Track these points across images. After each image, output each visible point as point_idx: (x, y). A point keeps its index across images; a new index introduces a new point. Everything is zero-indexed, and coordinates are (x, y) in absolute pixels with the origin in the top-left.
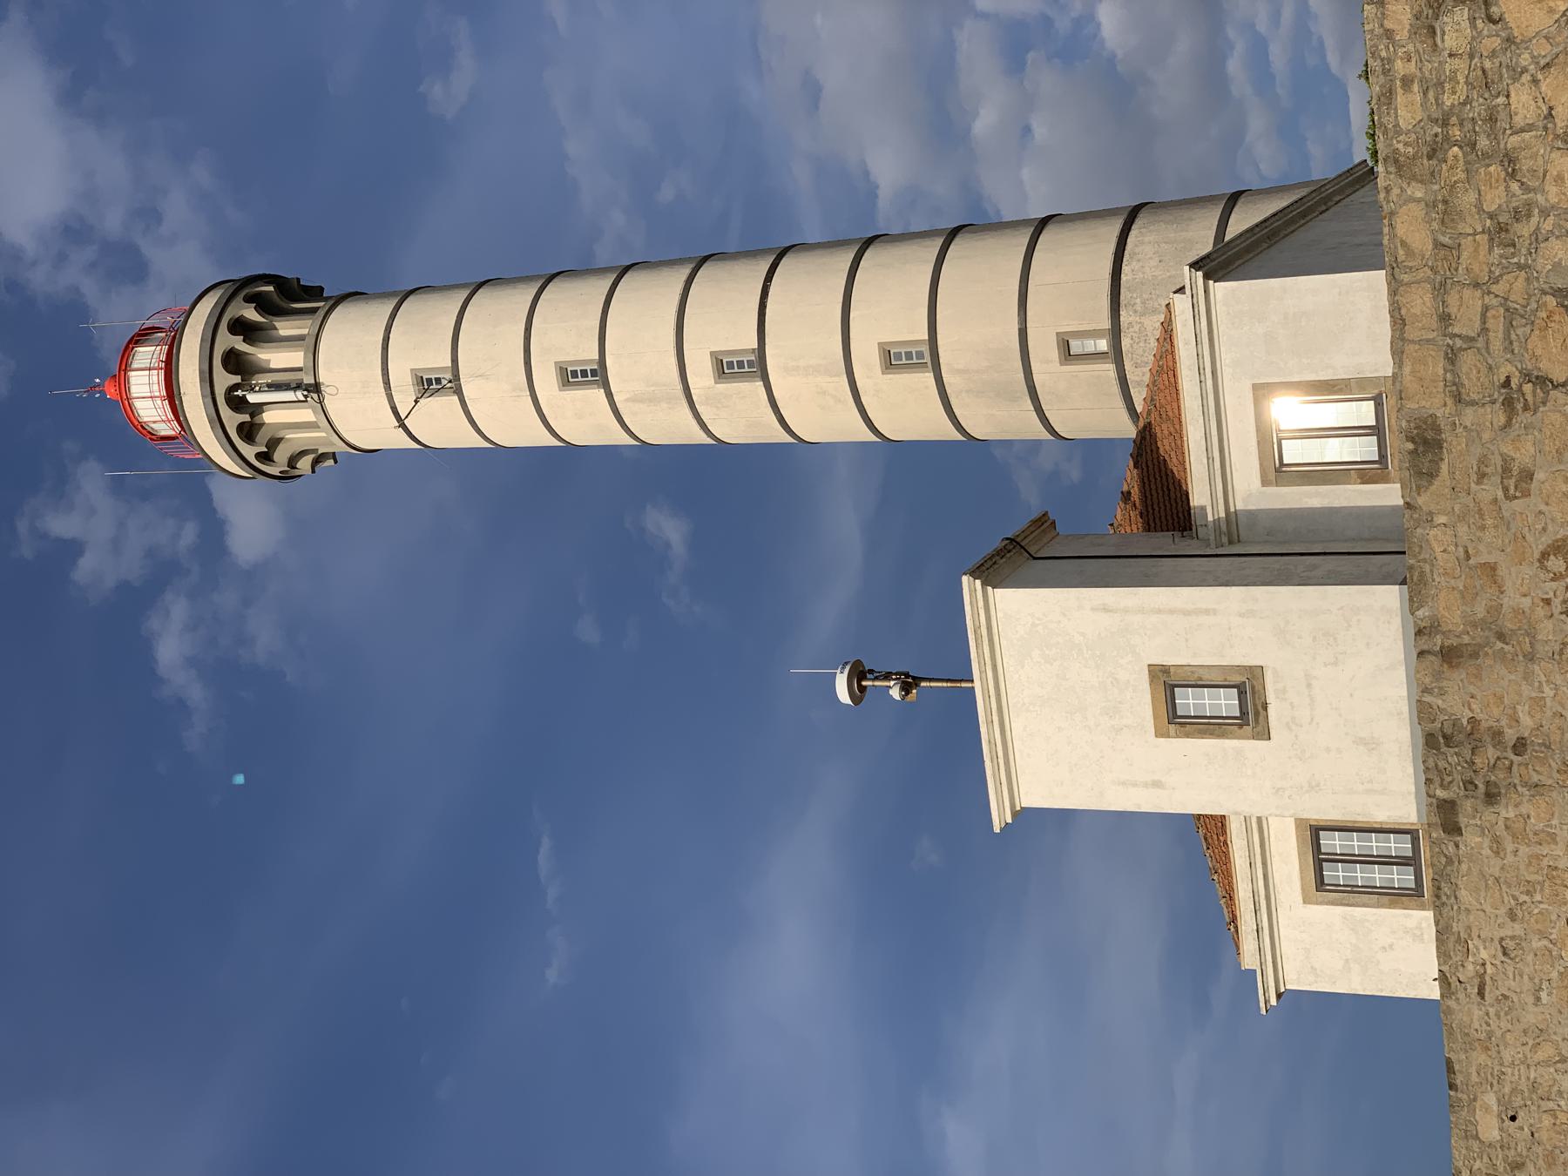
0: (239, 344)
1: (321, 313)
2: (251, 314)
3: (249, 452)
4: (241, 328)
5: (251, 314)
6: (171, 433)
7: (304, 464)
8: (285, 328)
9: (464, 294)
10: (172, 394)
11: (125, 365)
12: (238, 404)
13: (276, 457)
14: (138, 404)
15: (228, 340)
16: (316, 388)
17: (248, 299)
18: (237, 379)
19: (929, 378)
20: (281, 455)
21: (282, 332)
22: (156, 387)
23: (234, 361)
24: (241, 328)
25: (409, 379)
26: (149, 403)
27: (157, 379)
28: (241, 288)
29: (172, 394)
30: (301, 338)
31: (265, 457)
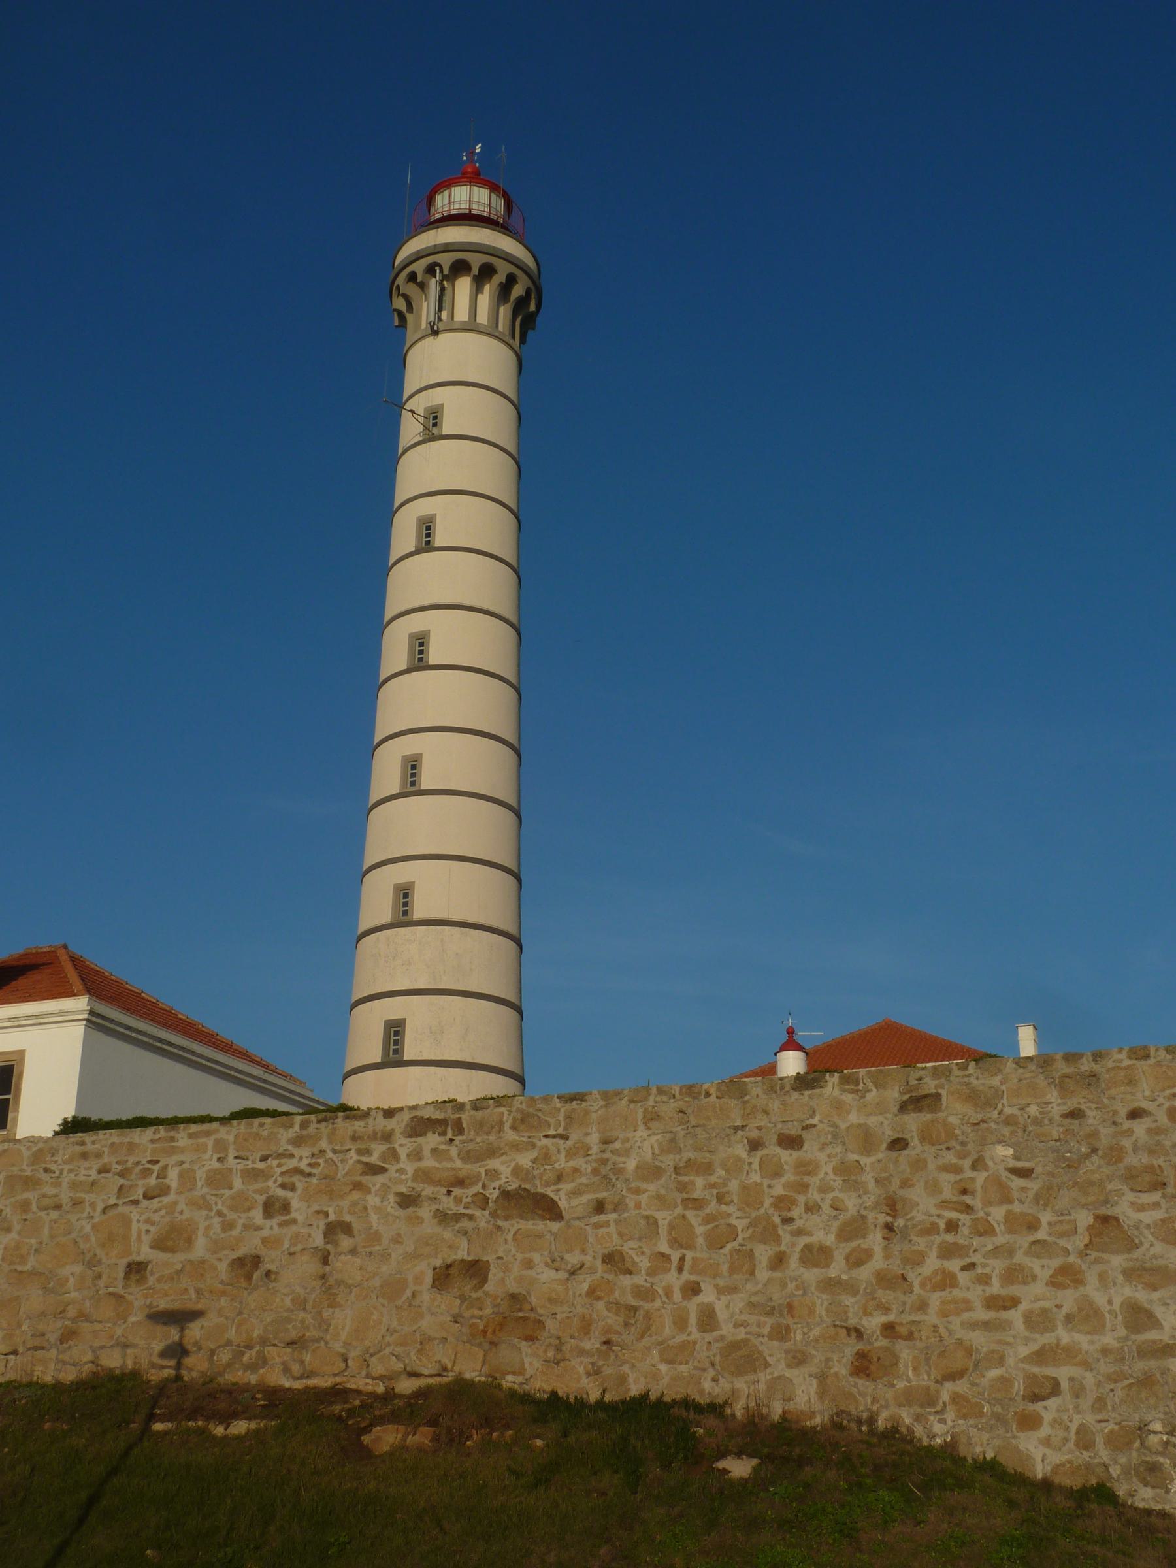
0: (500, 278)
1: (511, 341)
2: (518, 291)
3: (419, 267)
4: (511, 280)
5: (518, 291)
6: (432, 211)
7: (399, 304)
8: (505, 312)
9: (514, 452)
10: (469, 219)
11: (494, 188)
12: (430, 270)
13: (411, 285)
14: (446, 193)
15: (503, 270)
16: (435, 333)
17: (528, 291)
18: (446, 272)
19: (396, 791)
20: (411, 290)
21: (502, 309)
22: (456, 207)
23: (487, 272)
24: (511, 280)
25: (436, 402)
26: (446, 201)
27: (480, 209)
28: (536, 290)
29: (469, 219)
30: (497, 326)
31: (412, 277)
